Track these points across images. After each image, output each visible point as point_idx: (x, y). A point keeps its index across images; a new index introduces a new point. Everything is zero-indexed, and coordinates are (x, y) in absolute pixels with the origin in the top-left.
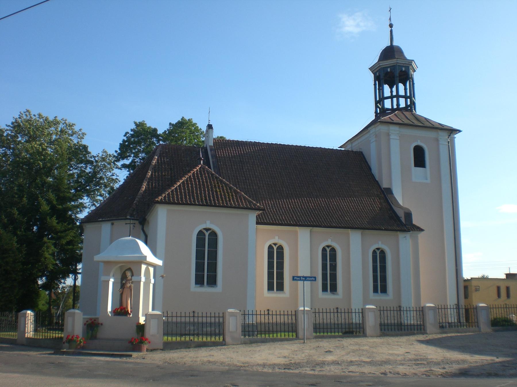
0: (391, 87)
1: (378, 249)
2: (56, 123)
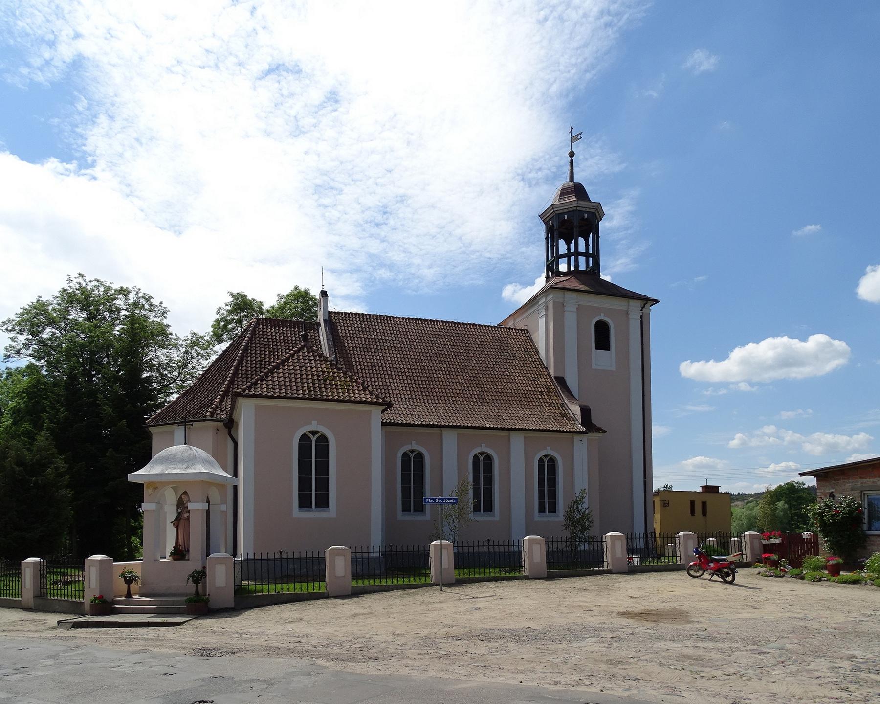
0: (568, 244)
1: (546, 456)
2: (124, 292)
